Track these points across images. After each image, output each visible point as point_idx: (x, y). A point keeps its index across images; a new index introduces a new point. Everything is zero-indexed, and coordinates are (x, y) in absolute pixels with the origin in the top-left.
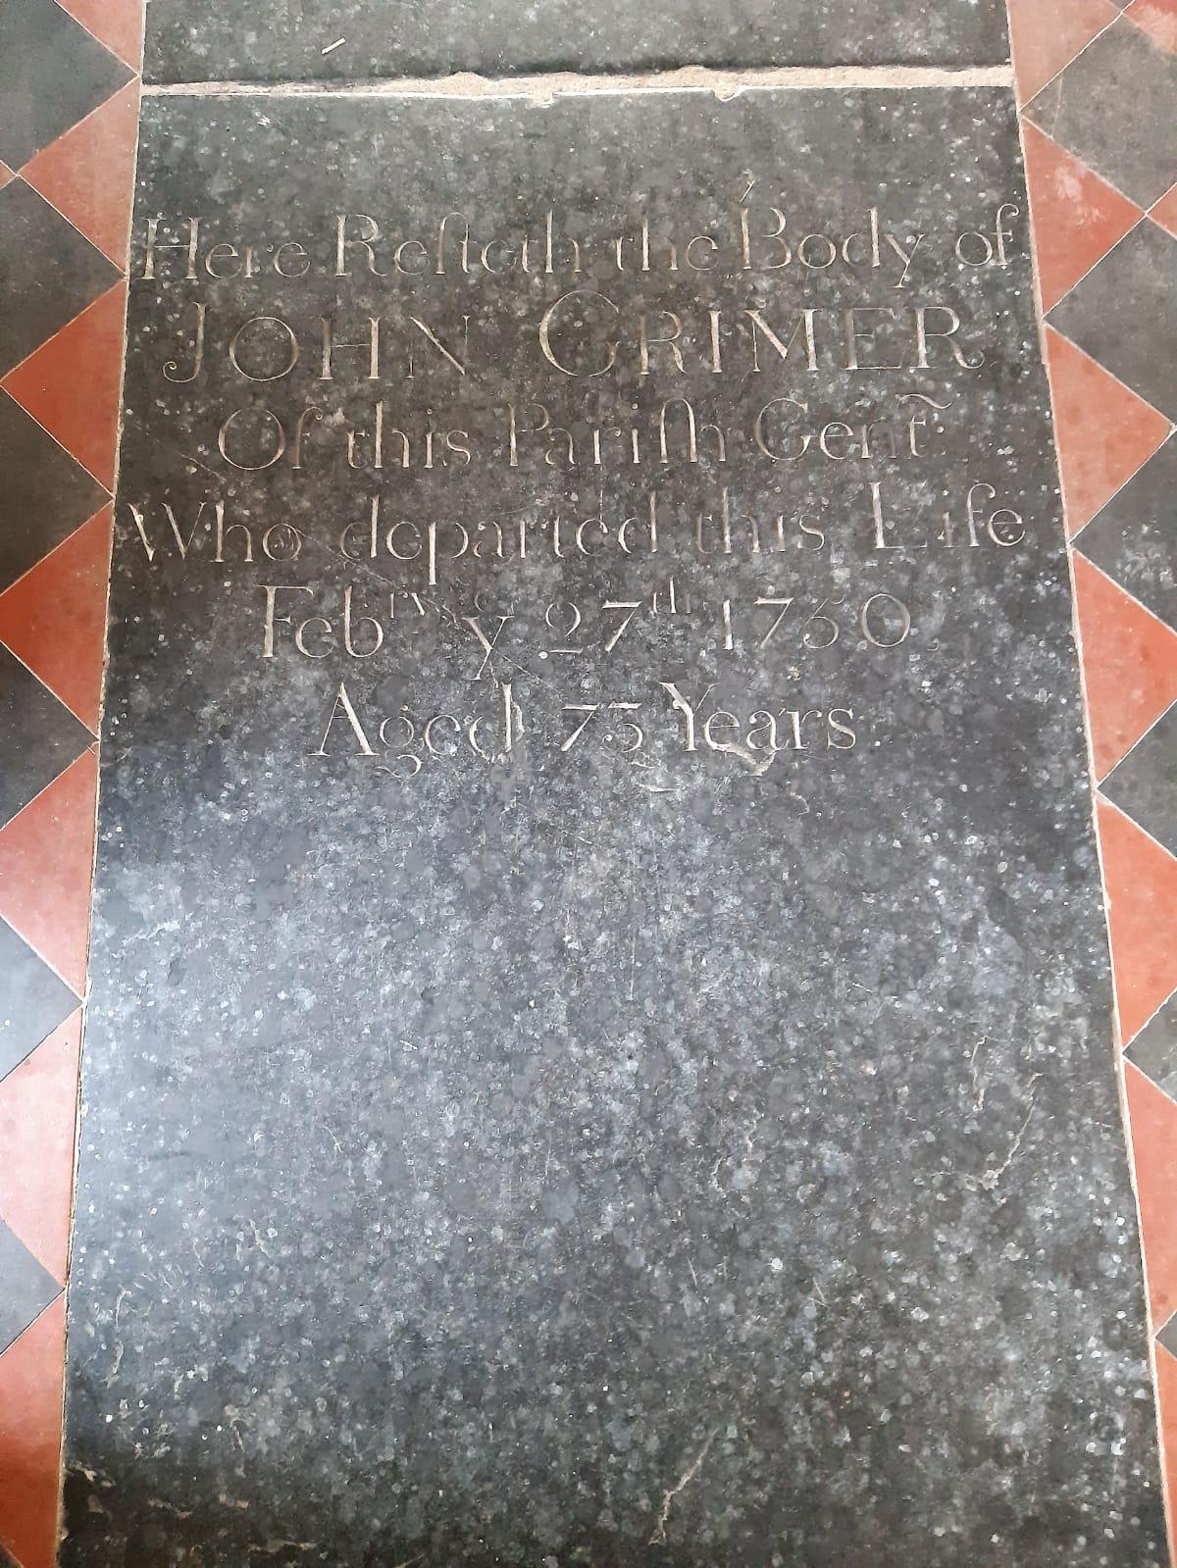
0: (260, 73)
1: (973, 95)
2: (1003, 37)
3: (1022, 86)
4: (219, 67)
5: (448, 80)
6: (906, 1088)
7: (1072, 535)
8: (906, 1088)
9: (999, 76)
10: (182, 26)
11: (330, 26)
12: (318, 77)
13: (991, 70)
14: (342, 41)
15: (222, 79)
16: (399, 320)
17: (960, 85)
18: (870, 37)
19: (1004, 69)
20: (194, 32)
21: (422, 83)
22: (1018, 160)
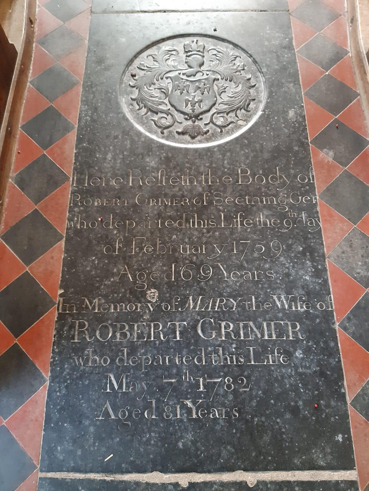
0: (82, 469)
1: (342, 485)
2: (352, 457)
3: (360, 480)
4: (68, 465)
5: (149, 474)
6: (301, 249)
7: (350, 399)
8: (301, 249)
9: (350, 475)
10: (55, 446)
11: (108, 447)
12: (103, 472)
13: (349, 472)
14: (112, 455)
15: (68, 471)
16: (271, 117)
17: (337, 479)
18: (304, 457)
19: (353, 471)
20: (59, 448)
21: (141, 475)
22: (343, 391)
